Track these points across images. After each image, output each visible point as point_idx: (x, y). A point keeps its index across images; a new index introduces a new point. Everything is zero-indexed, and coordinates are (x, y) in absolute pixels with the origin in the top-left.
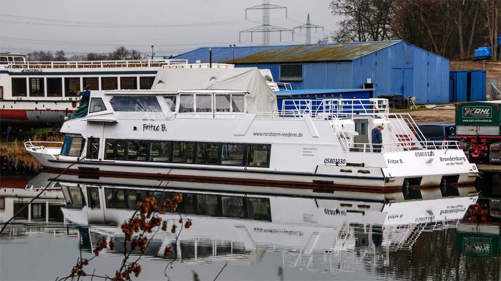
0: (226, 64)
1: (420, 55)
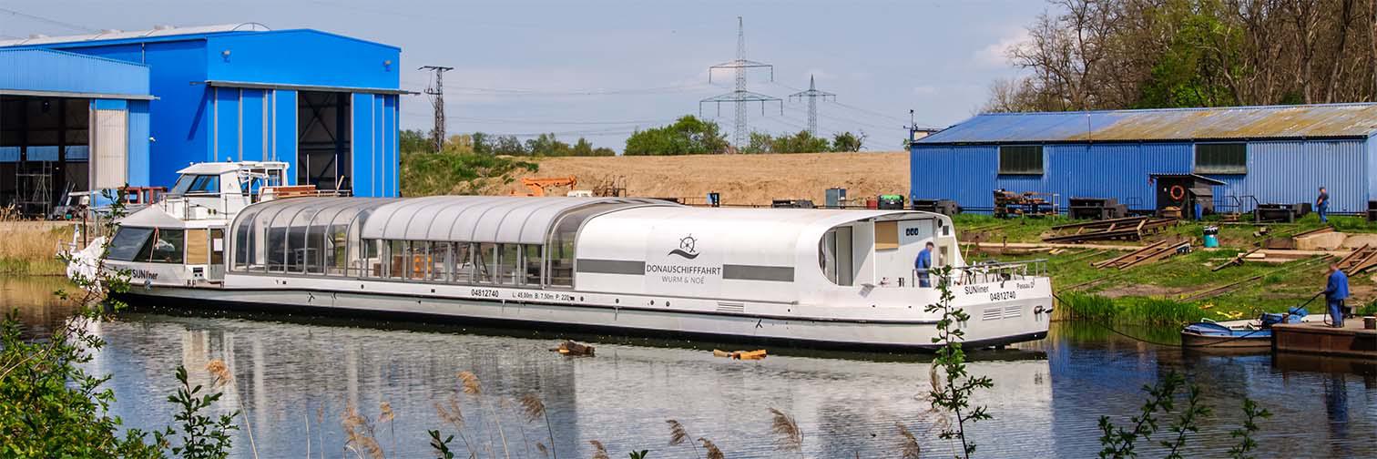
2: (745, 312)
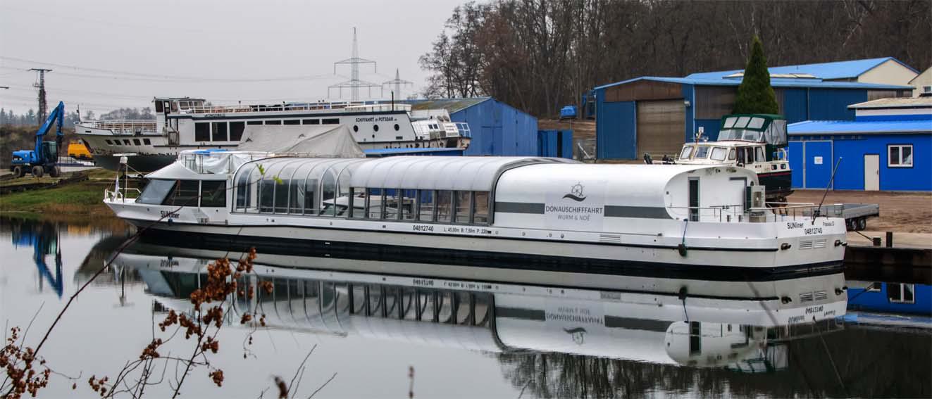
0: (403, 105)
1: (509, 112)
2: (622, 242)
